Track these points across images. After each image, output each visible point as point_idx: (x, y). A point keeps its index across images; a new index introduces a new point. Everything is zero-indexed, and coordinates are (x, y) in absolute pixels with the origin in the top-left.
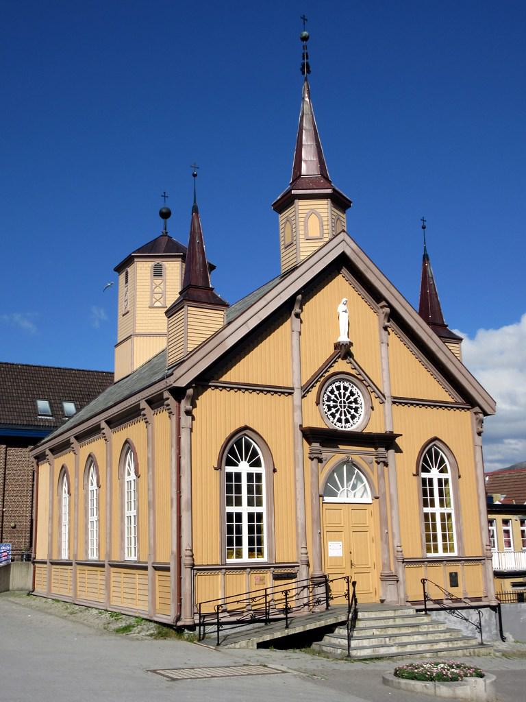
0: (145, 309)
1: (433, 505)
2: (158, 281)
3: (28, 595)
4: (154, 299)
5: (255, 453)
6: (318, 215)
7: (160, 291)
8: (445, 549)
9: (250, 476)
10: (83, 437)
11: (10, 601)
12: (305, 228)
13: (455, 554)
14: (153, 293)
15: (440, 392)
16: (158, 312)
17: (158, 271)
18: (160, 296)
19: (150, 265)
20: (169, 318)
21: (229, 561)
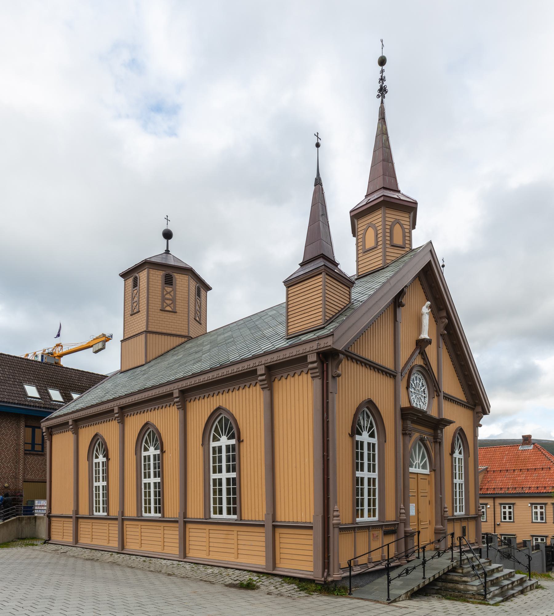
0: (156, 311)
1: (228, 480)
3: (45, 543)
4: (165, 304)
5: (231, 428)
6: (401, 225)
7: (171, 297)
10: (457, 356)
11: (397, 606)
12: (391, 234)
14: (164, 299)
16: (169, 315)
18: (171, 302)
19: (161, 274)
20: (288, 287)
21: (359, 520)
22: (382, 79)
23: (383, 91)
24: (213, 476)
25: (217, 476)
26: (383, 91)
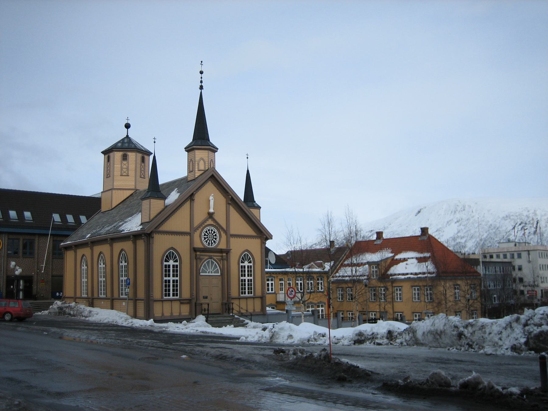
2: (125, 162)
5: (176, 257)
9: (173, 266)
17: (125, 158)
22: (201, 82)
23: (201, 88)
24: (252, 278)
25: (175, 278)
26: (201, 88)
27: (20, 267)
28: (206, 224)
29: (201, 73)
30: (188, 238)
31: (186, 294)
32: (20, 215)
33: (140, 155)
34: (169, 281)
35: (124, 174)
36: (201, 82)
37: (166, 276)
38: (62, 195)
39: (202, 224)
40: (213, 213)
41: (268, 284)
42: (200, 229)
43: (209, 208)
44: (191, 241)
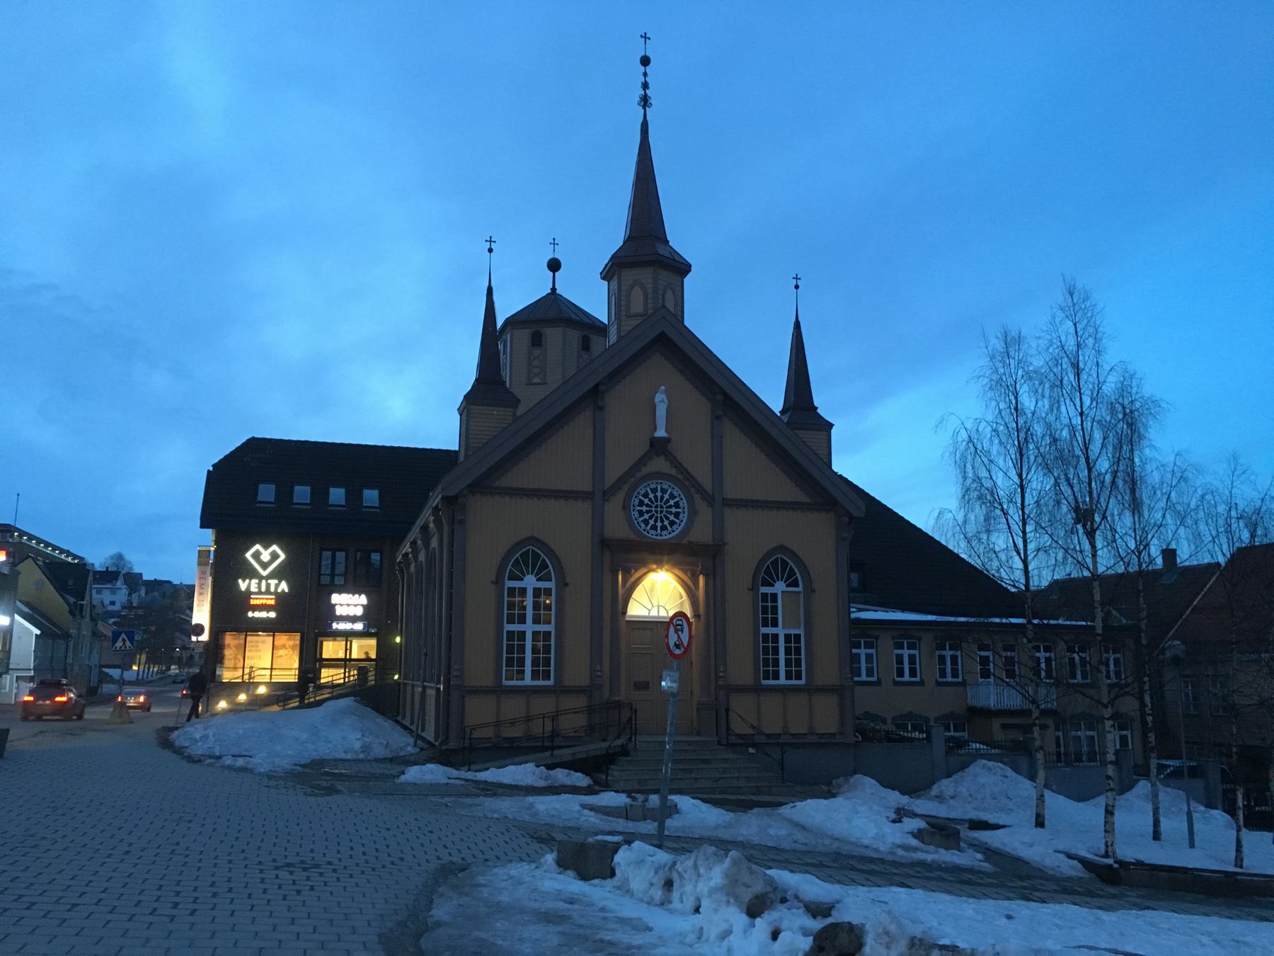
2: (537, 352)
5: (792, 573)
8: (789, 676)
13: (803, 682)
15: (786, 489)
17: (537, 340)
22: (645, 86)
23: (645, 101)
26: (645, 101)
27: (330, 613)
28: (639, 475)
29: (645, 61)
30: (584, 508)
31: (578, 674)
32: (354, 497)
33: (575, 335)
34: (522, 635)
35: (536, 380)
36: (645, 86)
37: (510, 621)
38: (432, 450)
39: (631, 477)
40: (665, 441)
41: (900, 659)
42: (626, 487)
43: (655, 429)
44: (598, 519)
